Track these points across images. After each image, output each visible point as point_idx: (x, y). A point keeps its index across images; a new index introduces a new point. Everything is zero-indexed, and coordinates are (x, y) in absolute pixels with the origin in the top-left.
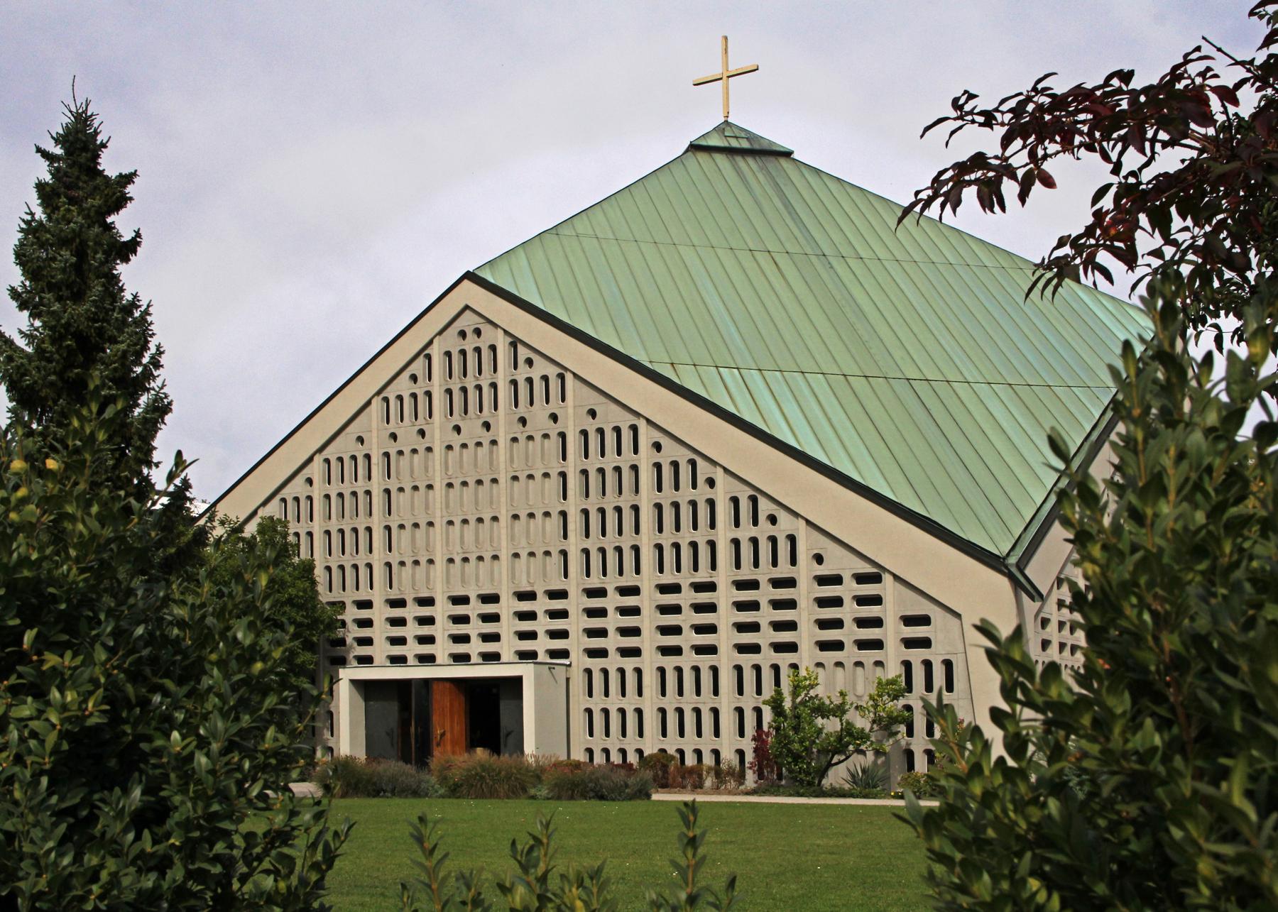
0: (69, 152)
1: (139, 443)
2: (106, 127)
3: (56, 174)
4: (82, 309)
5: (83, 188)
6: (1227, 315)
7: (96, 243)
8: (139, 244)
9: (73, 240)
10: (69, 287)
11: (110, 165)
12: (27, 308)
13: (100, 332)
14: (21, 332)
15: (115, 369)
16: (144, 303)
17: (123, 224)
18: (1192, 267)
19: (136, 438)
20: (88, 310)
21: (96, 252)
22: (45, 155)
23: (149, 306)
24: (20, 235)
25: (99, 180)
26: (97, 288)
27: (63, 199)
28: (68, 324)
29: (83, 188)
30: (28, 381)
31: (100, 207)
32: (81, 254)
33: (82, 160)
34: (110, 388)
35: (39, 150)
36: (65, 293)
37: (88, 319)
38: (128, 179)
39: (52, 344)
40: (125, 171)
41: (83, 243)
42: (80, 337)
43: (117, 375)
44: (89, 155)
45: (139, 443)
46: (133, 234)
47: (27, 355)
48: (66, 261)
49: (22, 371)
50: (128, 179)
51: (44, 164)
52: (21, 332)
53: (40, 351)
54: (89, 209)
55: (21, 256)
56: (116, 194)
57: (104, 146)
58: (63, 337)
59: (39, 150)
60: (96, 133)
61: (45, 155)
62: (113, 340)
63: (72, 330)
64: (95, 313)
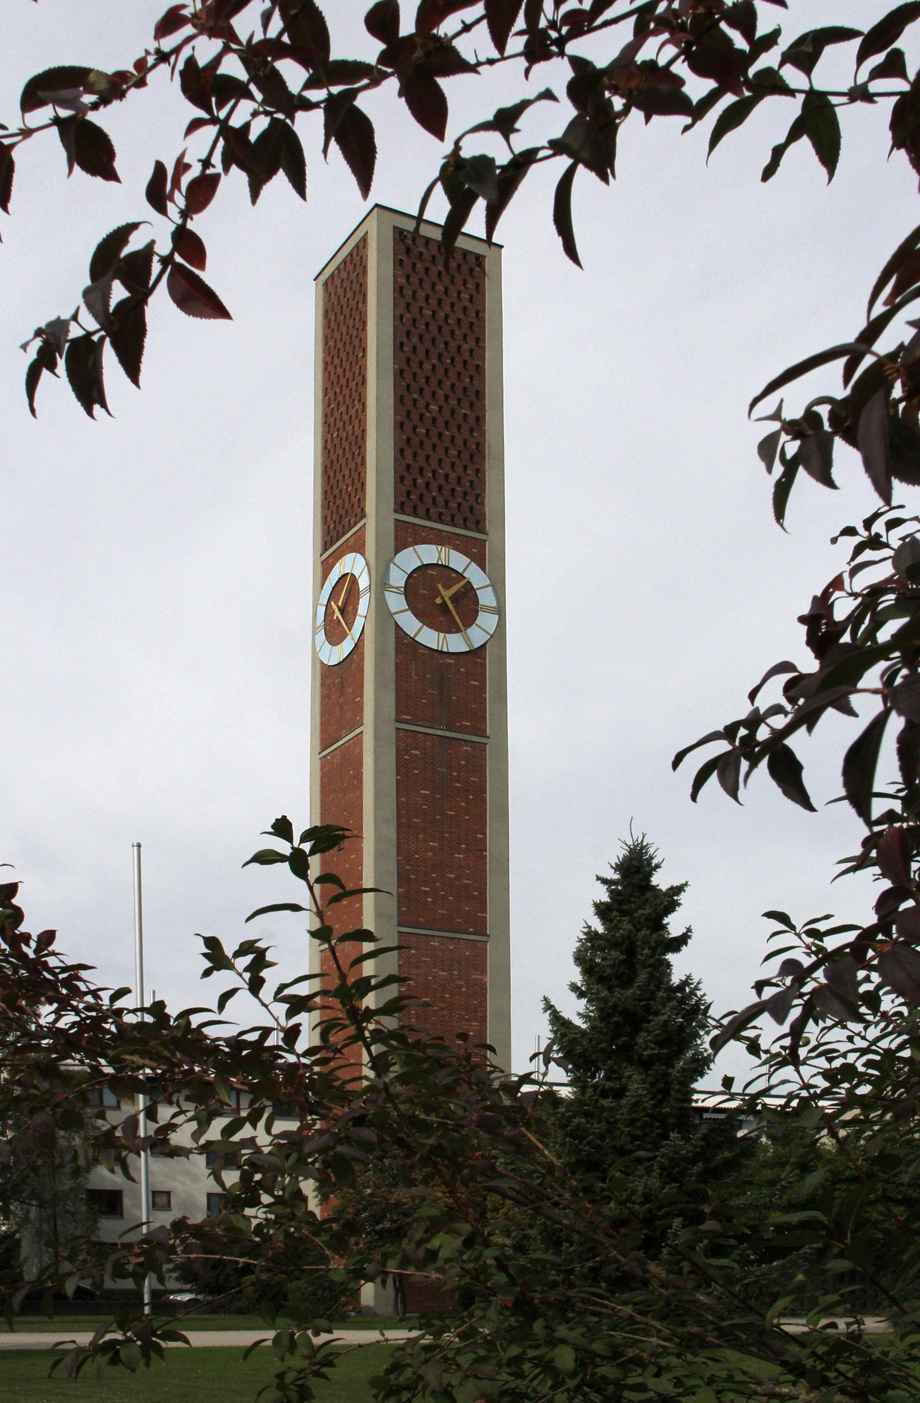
0: (624, 876)
1: (677, 1087)
2: (659, 851)
3: (612, 893)
4: (630, 992)
5: (634, 902)
6: (683, 61)
7: (644, 943)
8: (690, 937)
9: (623, 942)
10: (618, 978)
11: (661, 880)
12: (585, 997)
13: (647, 1009)
14: (579, 1014)
15: (658, 1035)
16: (696, 981)
17: (675, 924)
18: (485, 22)
19: (675, 1083)
20: (634, 993)
21: (643, 949)
22: (604, 881)
23: (698, 983)
24: (578, 944)
25: (649, 894)
26: (642, 976)
27: (615, 913)
28: (615, 1006)
29: (634, 902)
30: (579, 1049)
31: (649, 914)
32: (631, 952)
33: (635, 881)
34: (653, 1049)
35: (598, 878)
36: (615, 982)
37: (635, 1000)
38: (679, 890)
39: (601, 1021)
40: (676, 883)
41: (632, 944)
42: (625, 1013)
43: (659, 1039)
44: (641, 876)
45: (677, 1087)
46: (685, 931)
47: (583, 1033)
48: (616, 958)
49: (574, 1042)
50: (679, 890)
51: (604, 888)
52: (579, 1014)
53: (593, 1028)
54: (640, 917)
55: (579, 958)
56: (669, 901)
57: (658, 866)
58: (610, 1016)
59: (598, 878)
60: (651, 858)
61: (604, 881)
62: (657, 1013)
63: (619, 1009)
64: (640, 995)
